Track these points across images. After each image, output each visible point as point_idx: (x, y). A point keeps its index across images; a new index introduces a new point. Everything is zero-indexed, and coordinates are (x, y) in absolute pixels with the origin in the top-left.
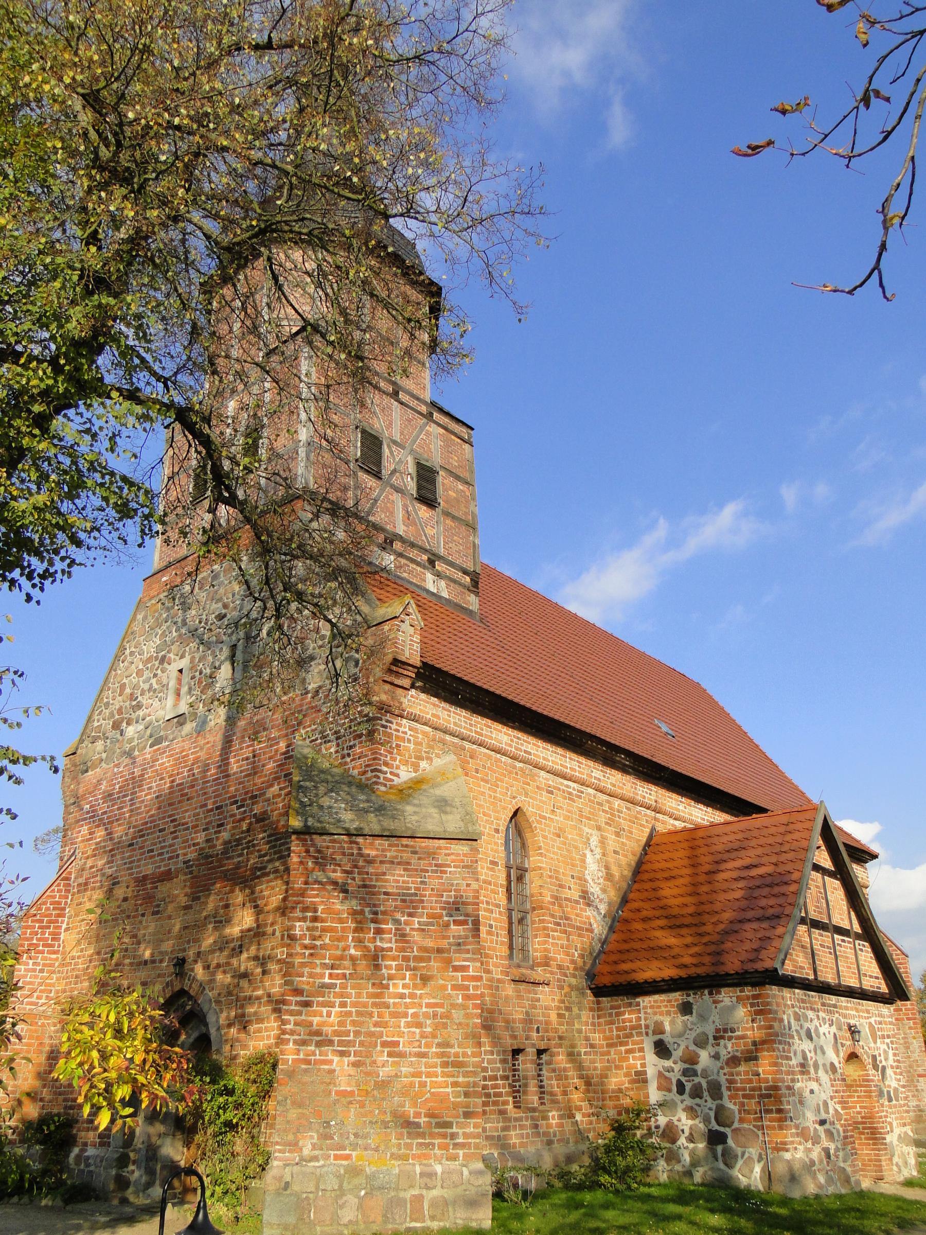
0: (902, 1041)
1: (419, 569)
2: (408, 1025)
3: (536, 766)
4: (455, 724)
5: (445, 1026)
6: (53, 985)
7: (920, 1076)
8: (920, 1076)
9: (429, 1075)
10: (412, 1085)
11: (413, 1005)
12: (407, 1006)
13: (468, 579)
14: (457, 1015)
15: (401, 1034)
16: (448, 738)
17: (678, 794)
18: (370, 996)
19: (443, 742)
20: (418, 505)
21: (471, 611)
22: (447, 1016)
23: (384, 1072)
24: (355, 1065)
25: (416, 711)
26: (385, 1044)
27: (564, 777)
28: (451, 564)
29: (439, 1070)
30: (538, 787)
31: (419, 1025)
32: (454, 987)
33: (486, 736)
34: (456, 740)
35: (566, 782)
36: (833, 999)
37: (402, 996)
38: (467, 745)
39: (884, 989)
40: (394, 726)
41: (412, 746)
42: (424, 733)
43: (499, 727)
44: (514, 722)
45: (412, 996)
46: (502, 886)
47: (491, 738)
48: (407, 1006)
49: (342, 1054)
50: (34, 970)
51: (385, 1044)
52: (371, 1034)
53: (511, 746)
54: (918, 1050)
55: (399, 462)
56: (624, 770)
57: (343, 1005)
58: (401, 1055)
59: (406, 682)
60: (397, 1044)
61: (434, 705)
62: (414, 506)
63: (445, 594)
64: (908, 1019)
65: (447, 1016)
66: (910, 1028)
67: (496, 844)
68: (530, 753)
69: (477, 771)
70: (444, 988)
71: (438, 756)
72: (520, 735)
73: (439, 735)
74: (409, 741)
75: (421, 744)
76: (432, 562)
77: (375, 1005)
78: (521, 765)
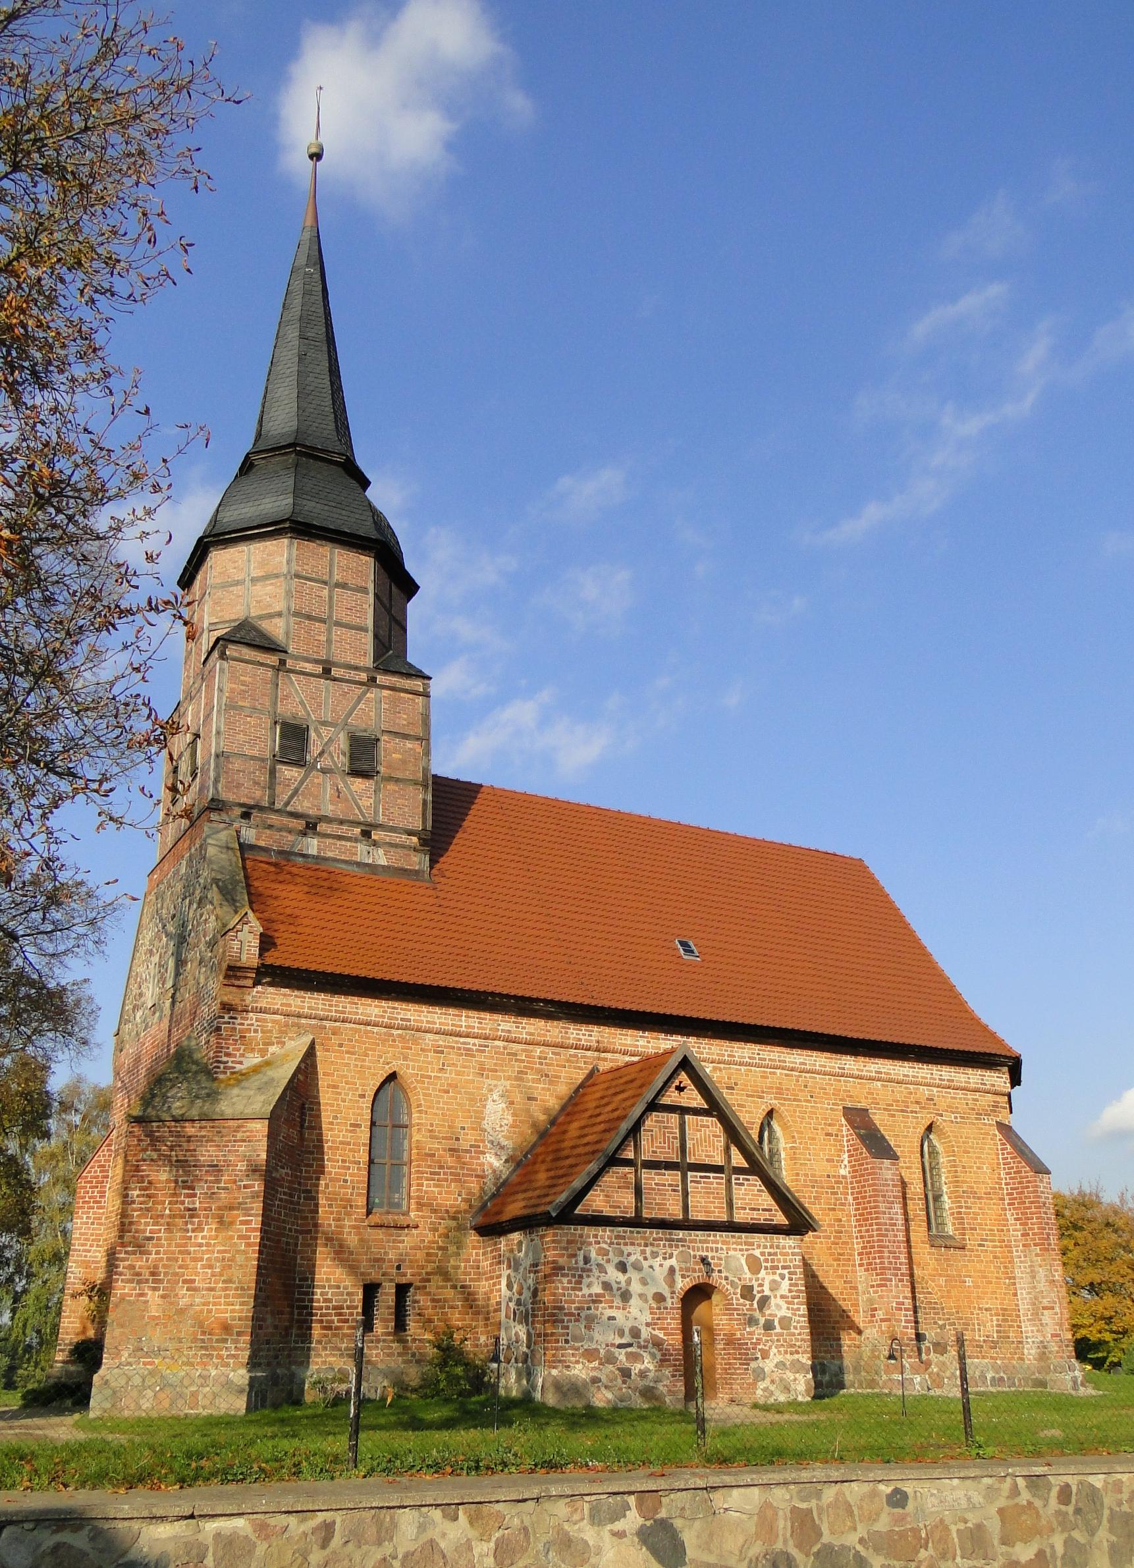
0: (1028, 1270)
1: (349, 844)
2: (203, 1267)
3: (418, 1030)
4: (309, 1008)
5: (230, 1267)
6: (101, 1235)
7: (1044, 1308)
8: (1044, 1308)
9: (215, 1304)
10: (202, 1311)
11: (208, 1252)
12: (203, 1253)
13: (415, 839)
14: (240, 1259)
15: (197, 1274)
16: (303, 1021)
17: (638, 1029)
18: (177, 1245)
19: (299, 1026)
20: (350, 780)
21: (417, 872)
22: (232, 1259)
23: (182, 1302)
24: (163, 1297)
25: (262, 1004)
26: (185, 1282)
27: (459, 1035)
28: (393, 829)
29: (222, 1300)
30: (422, 1050)
31: (210, 1267)
32: (240, 1237)
33: (350, 1013)
34: (313, 1022)
35: (462, 1040)
36: (681, 1234)
37: (200, 1245)
38: (327, 1024)
39: (780, 1219)
40: (239, 1021)
41: (260, 1035)
42: (273, 1021)
43: (369, 1001)
44: (389, 994)
45: (208, 1245)
46: (364, 1145)
47: (357, 1013)
48: (203, 1253)
49: (155, 1289)
50: (87, 1223)
51: (185, 1282)
52: (176, 1274)
53: (383, 1017)
54: (1043, 1280)
55: (328, 745)
56: (549, 1017)
57: (158, 1253)
58: (196, 1289)
59: (249, 982)
60: (193, 1281)
61: (285, 995)
62: (345, 783)
63: (383, 861)
64: (1035, 1245)
65: (232, 1259)
66: (1037, 1255)
67: (362, 1108)
68: (409, 1020)
69: (341, 1045)
70: (232, 1237)
71: (291, 1039)
72: (396, 1005)
73: (291, 1020)
74: (256, 1031)
75: (271, 1031)
76: (366, 834)
77: (180, 1252)
78: (400, 1032)
